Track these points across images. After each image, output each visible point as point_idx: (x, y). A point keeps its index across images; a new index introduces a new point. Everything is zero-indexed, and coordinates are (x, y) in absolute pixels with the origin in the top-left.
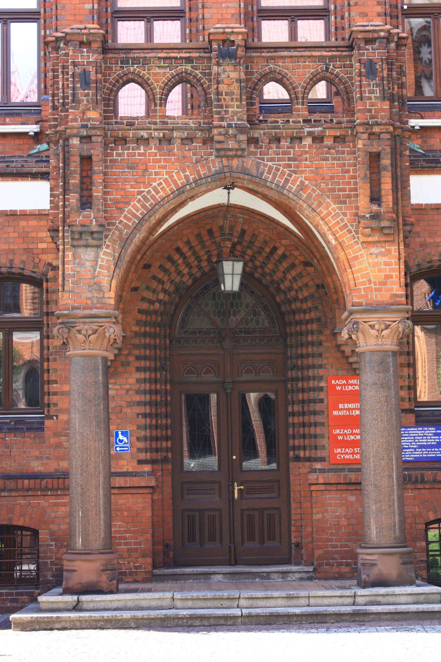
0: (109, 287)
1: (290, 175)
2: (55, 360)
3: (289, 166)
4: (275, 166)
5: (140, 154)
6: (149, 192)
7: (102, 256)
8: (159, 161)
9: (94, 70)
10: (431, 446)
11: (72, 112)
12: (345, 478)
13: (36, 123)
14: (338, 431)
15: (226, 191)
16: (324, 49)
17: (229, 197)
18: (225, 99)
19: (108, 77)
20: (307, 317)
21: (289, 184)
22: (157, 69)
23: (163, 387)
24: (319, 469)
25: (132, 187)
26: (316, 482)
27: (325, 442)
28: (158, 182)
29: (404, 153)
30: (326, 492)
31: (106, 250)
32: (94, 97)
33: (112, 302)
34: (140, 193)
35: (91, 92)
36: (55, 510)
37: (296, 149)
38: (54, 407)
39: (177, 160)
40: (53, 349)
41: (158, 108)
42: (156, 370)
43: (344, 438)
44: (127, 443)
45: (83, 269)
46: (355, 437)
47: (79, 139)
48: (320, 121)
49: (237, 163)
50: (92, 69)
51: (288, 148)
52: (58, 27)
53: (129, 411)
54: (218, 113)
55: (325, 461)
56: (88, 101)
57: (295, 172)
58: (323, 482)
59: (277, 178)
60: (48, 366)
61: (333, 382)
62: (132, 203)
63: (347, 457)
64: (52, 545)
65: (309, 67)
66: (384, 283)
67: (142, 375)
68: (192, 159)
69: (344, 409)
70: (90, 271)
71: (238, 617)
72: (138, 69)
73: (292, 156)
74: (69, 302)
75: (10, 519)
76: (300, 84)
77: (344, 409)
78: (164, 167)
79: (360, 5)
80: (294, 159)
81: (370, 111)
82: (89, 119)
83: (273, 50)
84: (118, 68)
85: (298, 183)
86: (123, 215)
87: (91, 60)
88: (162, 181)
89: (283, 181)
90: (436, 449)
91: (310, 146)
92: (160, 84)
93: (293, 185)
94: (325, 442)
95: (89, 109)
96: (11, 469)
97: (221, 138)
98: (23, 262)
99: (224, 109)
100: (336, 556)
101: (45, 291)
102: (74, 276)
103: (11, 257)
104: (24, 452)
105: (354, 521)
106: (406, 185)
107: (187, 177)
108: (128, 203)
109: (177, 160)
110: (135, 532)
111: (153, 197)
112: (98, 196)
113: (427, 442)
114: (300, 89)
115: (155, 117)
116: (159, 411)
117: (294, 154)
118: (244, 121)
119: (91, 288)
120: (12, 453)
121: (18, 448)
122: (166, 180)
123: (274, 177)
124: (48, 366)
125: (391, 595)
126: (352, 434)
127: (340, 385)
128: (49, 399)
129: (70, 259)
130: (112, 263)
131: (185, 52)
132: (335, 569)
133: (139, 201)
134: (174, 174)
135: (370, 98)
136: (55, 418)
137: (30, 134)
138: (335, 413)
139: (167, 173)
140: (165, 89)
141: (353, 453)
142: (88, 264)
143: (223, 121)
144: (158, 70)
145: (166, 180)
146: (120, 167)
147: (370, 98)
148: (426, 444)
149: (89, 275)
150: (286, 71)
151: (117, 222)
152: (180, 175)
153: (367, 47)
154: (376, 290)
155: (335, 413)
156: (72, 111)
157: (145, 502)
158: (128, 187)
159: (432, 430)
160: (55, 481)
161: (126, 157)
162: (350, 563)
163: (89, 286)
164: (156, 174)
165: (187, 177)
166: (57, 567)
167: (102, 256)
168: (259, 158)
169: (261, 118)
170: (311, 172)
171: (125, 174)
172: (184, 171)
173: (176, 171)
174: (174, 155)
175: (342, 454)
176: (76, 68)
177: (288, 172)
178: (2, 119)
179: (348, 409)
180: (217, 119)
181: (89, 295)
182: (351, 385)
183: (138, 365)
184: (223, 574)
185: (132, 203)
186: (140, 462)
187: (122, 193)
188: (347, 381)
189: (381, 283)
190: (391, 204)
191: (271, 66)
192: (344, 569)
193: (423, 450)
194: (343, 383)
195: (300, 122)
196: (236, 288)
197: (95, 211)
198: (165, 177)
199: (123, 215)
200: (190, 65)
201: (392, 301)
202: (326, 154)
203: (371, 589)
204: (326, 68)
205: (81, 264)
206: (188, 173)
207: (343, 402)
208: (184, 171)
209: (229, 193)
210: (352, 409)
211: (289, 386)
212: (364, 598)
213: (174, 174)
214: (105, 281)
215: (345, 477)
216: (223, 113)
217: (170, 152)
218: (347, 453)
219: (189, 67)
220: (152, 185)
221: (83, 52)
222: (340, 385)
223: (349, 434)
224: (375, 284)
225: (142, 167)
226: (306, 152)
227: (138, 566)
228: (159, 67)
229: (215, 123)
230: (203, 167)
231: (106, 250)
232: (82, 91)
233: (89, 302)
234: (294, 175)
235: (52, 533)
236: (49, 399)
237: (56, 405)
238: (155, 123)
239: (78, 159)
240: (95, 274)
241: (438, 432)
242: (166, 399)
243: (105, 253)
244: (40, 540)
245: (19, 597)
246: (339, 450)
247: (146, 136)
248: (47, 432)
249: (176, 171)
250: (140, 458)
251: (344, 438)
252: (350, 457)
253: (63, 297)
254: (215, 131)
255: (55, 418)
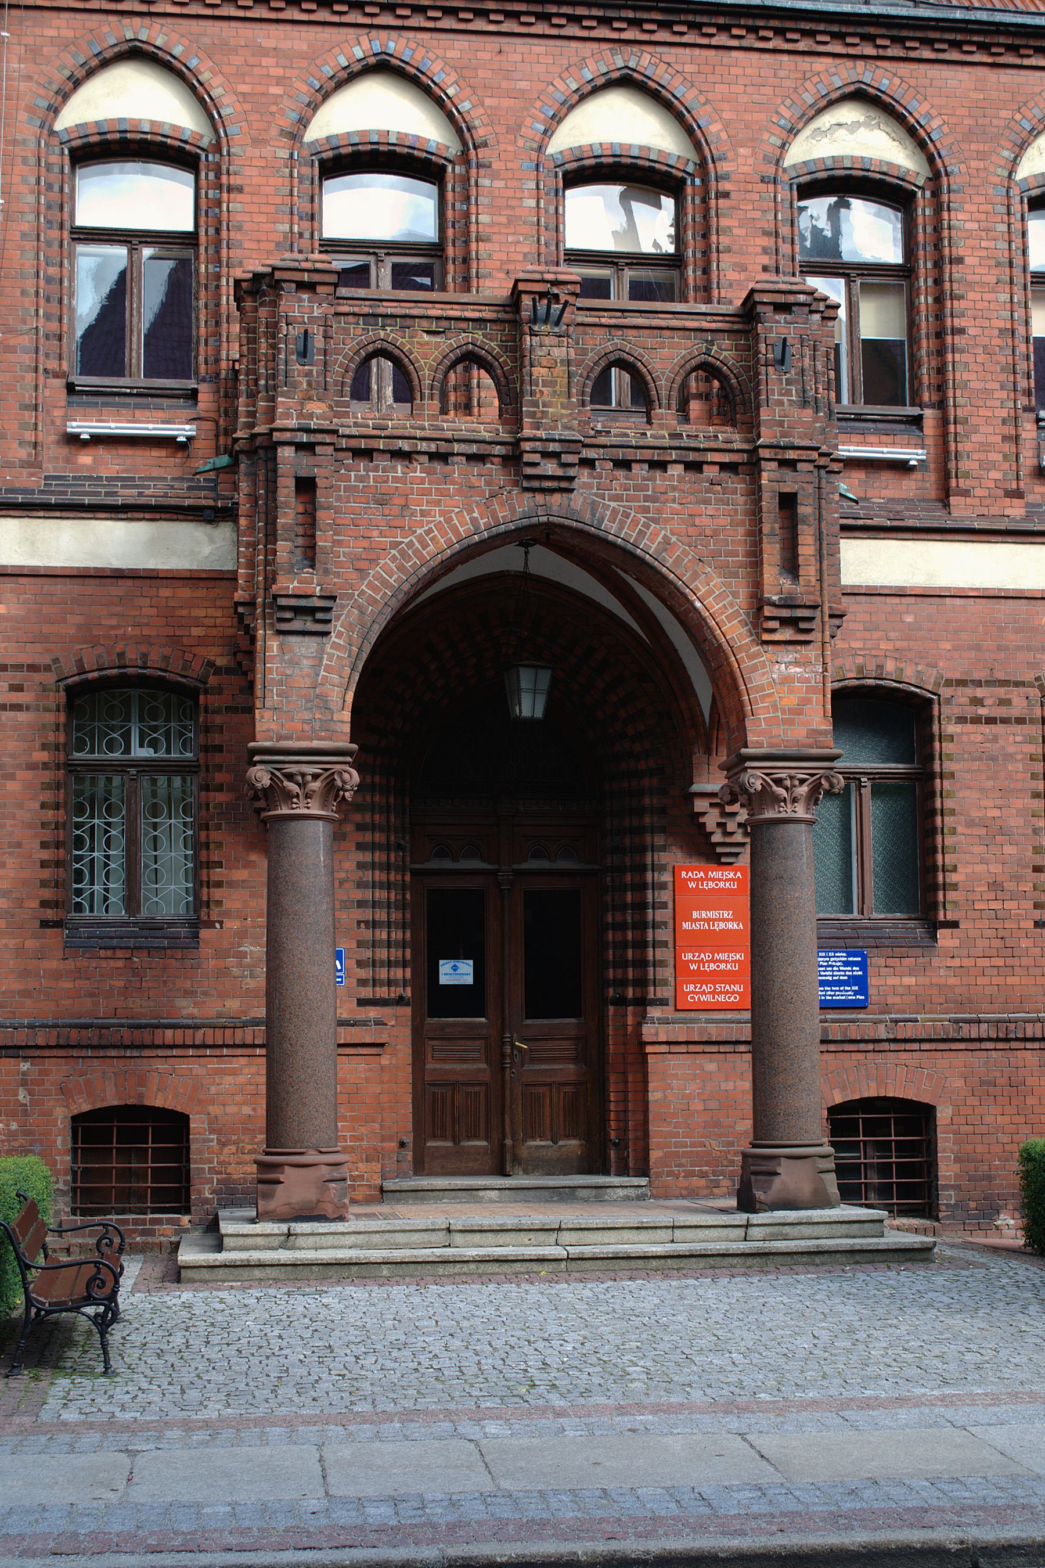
0: (341, 702)
1: (647, 526)
2: (219, 827)
3: (646, 510)
4: (622, 509)
5: (395, 479)
6: (411, 543)
7: (329, 650)
8: (427, 492)
9: (321, 333)
10: (839, 983)
11: (283, 402)
12: (700, 1034)
13: (190, 421)
14: (689, 956)
15: (523, 549)
16: (703, 317)
17: (526, 560)
18: (541, 392)
19: (342, 346)
20: (642, 766)
21: (645, 541)
22: (425, 335)
23: (399, 877)
24: (658, 1019)
25: (382, 534)
26: (655, 1040)
27: (666, 973)
28: (426, 528)
29: (831, 496)
30: (669, 1056)
31: (337, 640)
32: (321, 379)
33: (347, 728)
34: (395, 545)
35: (315, 369)
36: (217, 1081)
37: (658, 482)
38: (217, 906)
39: (458, 491)
40: (215, 808)
41: (426, 402)
42: (388, 848)
43: (699, 967)
44: (341, 971)
45: (297, 671)
46: (718, 966)
47: (293, 448)
48: (697, 436)
49: (559, 501)
50: (318, 330)
51: (644, 479)
52: (948, 169)
53: (345, 917)
54: (533, 415)
55: (667, 1005)
56: (309, 384)
57: (655, 521)
58: (665, 1040)
59: (625, 530)
60: (208, 836)
61: (684, 874)
62: (383, 562)
63: (703, 998)
64: (212, 1141)
65: (678, 346)
66: (800, 712)
67: (366, 857)
68: (484, 491)
69: (701, 920)
70: (309, 675)
71: (561, 1260)
72: (392, 335)
73: (650, 493)
74: (273, 726)
75: (141, 1096)
76: (663, 374)
77: (701, 920)
78: (438, 503)
79: (734, 253)
80: (654, 499)
81: (781, 424)
82: (311, 416)
83: (620, 314)
84: (359, 332)
85: (660, 539)
86: (366, 582)
87: (315, 314)
88: (432, 525)
89: (635, 535)
90: (847, 988)
91: (681, 479)
92: (430, 361)
93: (652, 541)
94: (666, 973)
95: (310, 399)
96: (143, 1010)
97: (536, 458)
98: (166, 658)
99: (541, 408)
100: (684, 1160)
101: (202, 710)
102: (280, 683)
103: (143, 649)
104: (165, 982)
105: (713, 1104)
106: (835, 552)
107: (474, 521)
108: (374, 561)
109: (458, 491)
110: (353, 1119)
111: (416, 552)
112: (325, 547)
113: (833, 976)
114: (663, 382)
115: (421, 416)
116: (393, 918)
117: (653, 491)
118: (574, 430)
119: (309, 705)
120: (144, 985)
121: (153, 976)
122: (439, 525)
123: (621, 529)
124: (208, 836)
125: (806, 1223)
126: (713, 961)
127: (694, 880)
128: (209, 893)
129: (275, 653)
130: (347, 662)
131: (473, 310)
132: (682, 1182)
133: (394, 559)
134: (453, 515)
135: (781, 403)
136: (218, 925)
137: (178, 440)
138: (686, 925)
139: (442, 513)
140: (439, 371)
141: (714, 993)
142: (305, 662)
143: (538, 429)
144: (426, 337)
145: (439, 525)
146: (363, 500)
147: (781, 403)
148: (830, 978)
149: (308, 682)
150: (642, 351)
151: (356, 593)
152: (463, 516)
153: (777, 317)
154: (785, 722)
155: (686, 925)
156: (283, 399)
157: (370, 1070)
158: (375, 533)
159: (842, 956)
160: (219, 1032)
161: (372, 483)
162: (707, 1172)
163: (307, 702)
164: (423, 513)
165: (474, 521)
166: (219, 1176)
167: (329, 650)
168: (595, 495)
169: (599, 427)
170: (683, 521)
171: (370, 512)
172: (470, 511)
173: (457, 510)
174: (453, 483)
175: (697, 993)
176: (290, 327)
177: (643, 520)
178: (130, 412)
179: (708, 920)
180: (529, 426)
181: (307, 716)
182: (713, 880)
183: (360, 840)
184: (499, 1189)
185: (383, 562)
186: (362, 1002)
187: (365, 543)
188: (706, 874)
189: (792, 711)
190: (813, 579)
191: (616, 341)
192: (697, 1182)
193: (827, 988)
194: (699, 876)
195: (664, 437)
196: (539, 714)
197: (321, 572)
198: (438, 519)
199: (366, 582)
200: (480, 333)
201: (811, 740)
202: (706, 492)
203: (768, 1214)
204: (707, 349)
205: (294, 663)
206: (476, 515)
207: (699, 909)
208: (470, 511)
209: (526, 553)
210: (714, 920)
211: (608, 879)
212: (762, 1228)
213: (453, 515)
214: (335, 695)
215: (702, 1031)
216: (539, 415)
217: (446, 478)
218: (704, 993)
219: (479, 336)
220: (415, 532)
221: (301, 300)
222: (694, 880)
223: (707, 961)
224: (783, 712)
225: (398, 501)
226: (674, 488)
227: (358, 1176)
228: (428, 332)
229: (527, 432)
230: (502, 505)
231: (337, 640)
232: (300, 367)
233: (307, 727)
234: (653, 525)
235: (213, 1120)
236: (209, 893)
237: (219, 903)
238: (423, 429)
239: (292, 483)
240: (317, 680)
241: (851, 959)
242: (404, 898)
243: (335, 646)
244: (191, 1132)
245: (156, 1227)
246: (692, 987)
247: (406, 448)
248: (205, 951)
249: (457, 510)
250: (362, 996)
251: (699, 967)
252: (709, 998)
253: (262, 717)
254: (527, 446)
255: (218, 925)
